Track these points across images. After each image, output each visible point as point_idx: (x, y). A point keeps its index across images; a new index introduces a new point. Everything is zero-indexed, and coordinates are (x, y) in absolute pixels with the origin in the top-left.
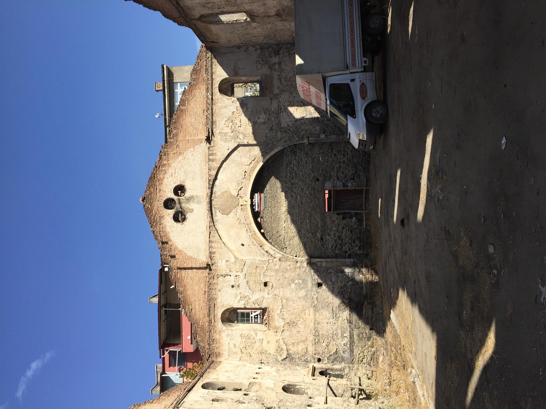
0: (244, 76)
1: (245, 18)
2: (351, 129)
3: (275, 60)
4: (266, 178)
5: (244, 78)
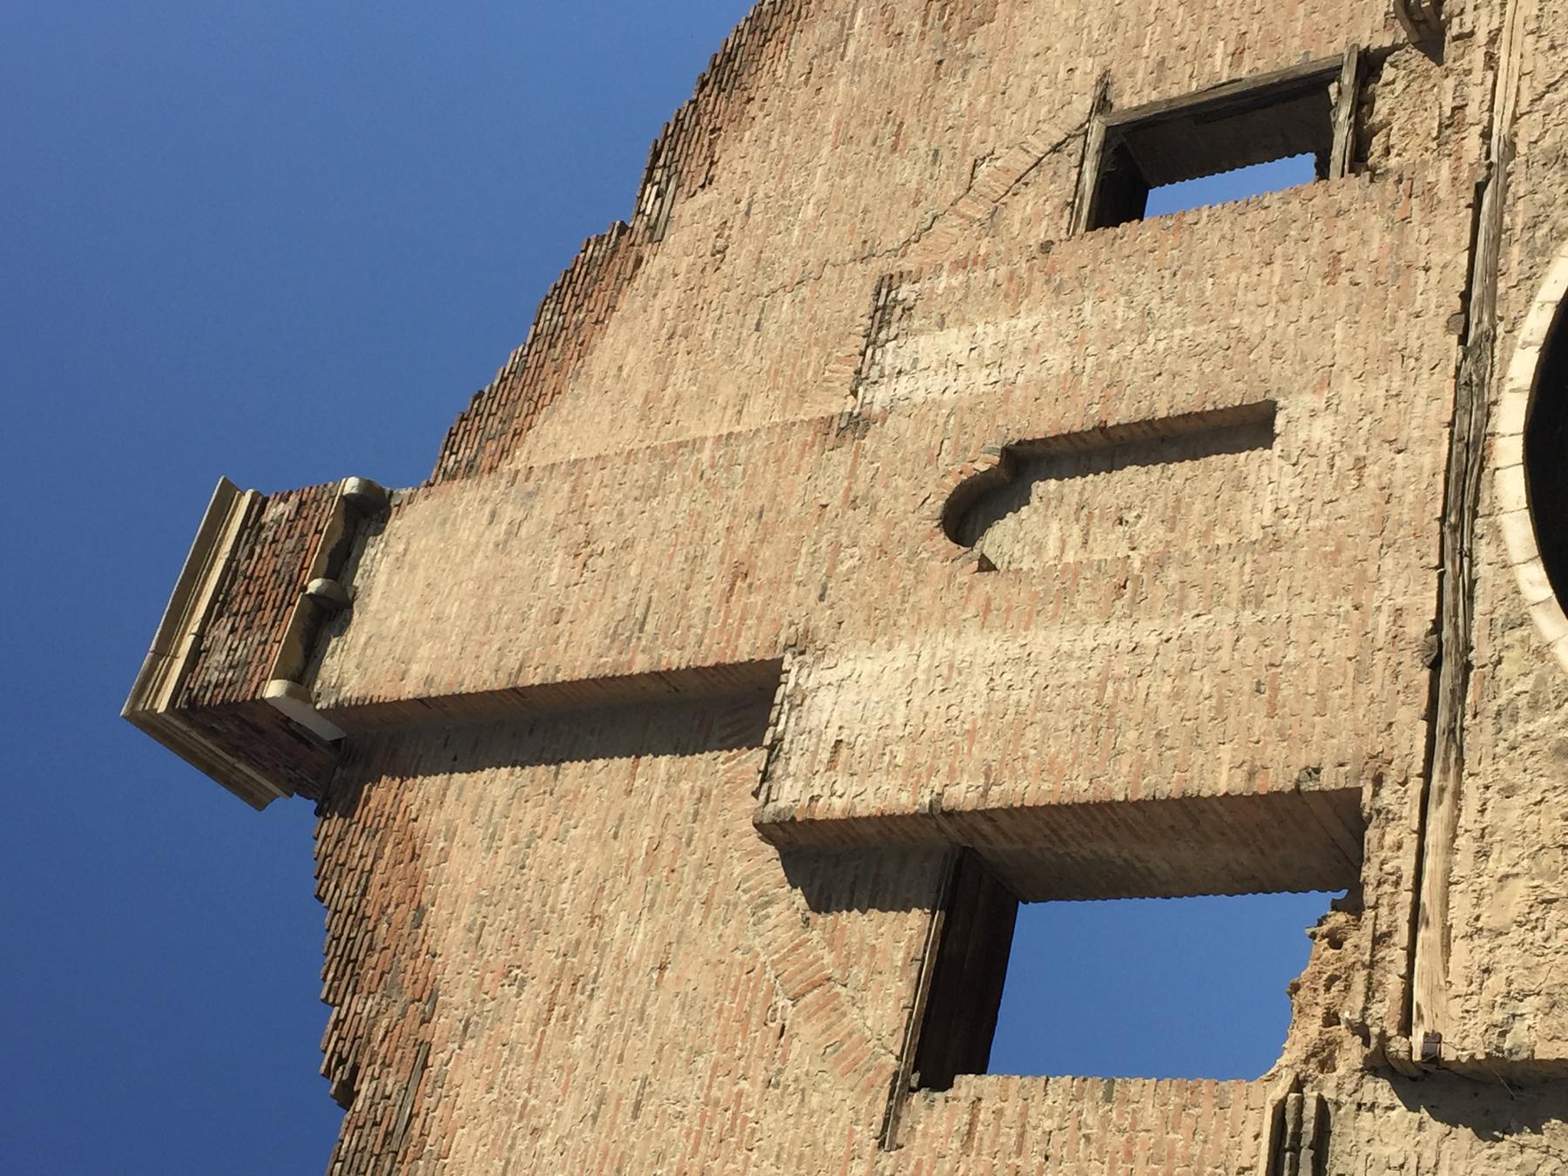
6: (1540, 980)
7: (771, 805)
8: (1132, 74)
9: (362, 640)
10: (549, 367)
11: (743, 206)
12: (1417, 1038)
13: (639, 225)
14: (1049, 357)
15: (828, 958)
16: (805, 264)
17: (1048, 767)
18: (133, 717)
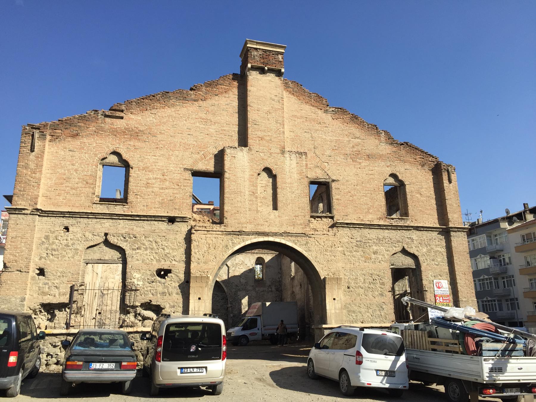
0: (266, 271)
1: (292, 275)
2: (236, 328)
3: (274, 289)
4: (61, 159)
5: (264, 271)
6: (200, 244)
7: (227, 149)
8: (338, 185)
9: (258, 77)
10: (304, 97)
11: (328, 126)
12: (194, 232)
13: (328, 108)
14: (289, 180)
15: (208, 158)
16: (315, 138)
17: (229, 186)
18: (246, 41)
